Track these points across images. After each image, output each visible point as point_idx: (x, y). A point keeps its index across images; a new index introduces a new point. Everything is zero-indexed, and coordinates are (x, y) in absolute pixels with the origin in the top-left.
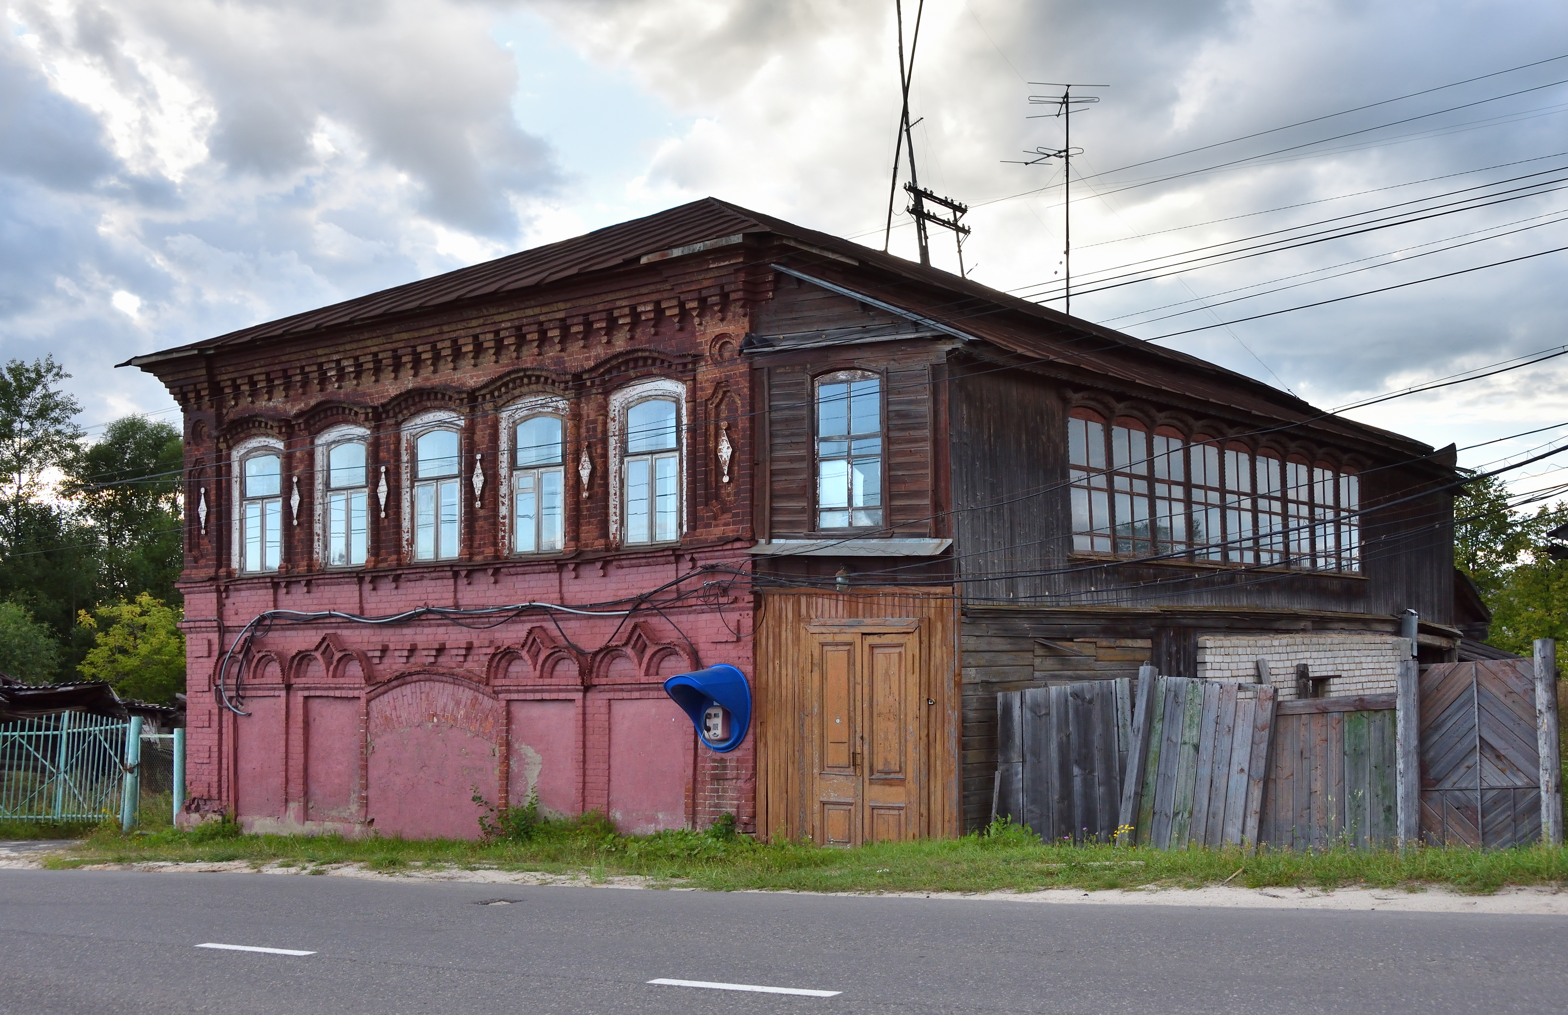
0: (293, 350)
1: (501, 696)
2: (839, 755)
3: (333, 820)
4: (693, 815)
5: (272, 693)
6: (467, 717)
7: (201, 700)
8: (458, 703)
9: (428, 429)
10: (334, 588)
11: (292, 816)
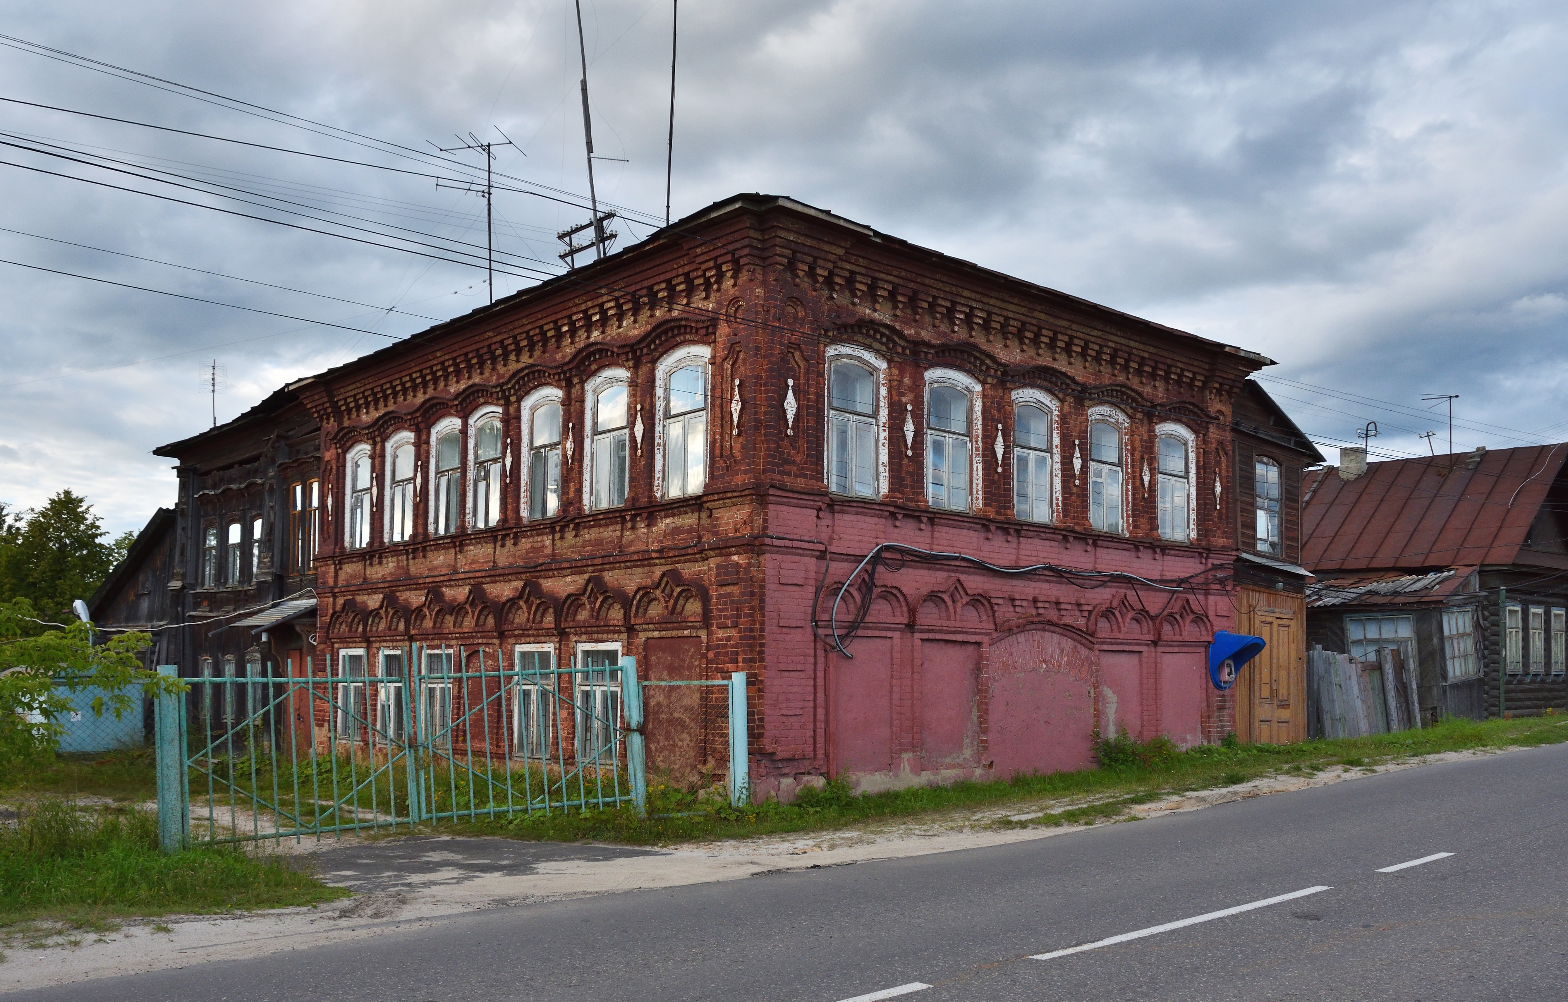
0: (944, 279)
1: (1096, 646)
2: (1266, 692)
3: (948, 767)
4: (1207, 736)
5: (884, 634)
6: (1069, 663)
7: (788, 638)
8: (1062, 651)
9: (679, 367)
10: (953, 531)
11: (908, 768)
